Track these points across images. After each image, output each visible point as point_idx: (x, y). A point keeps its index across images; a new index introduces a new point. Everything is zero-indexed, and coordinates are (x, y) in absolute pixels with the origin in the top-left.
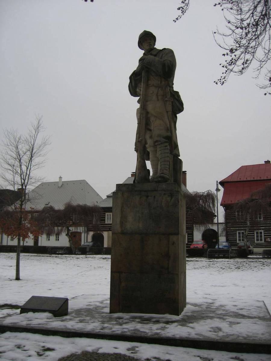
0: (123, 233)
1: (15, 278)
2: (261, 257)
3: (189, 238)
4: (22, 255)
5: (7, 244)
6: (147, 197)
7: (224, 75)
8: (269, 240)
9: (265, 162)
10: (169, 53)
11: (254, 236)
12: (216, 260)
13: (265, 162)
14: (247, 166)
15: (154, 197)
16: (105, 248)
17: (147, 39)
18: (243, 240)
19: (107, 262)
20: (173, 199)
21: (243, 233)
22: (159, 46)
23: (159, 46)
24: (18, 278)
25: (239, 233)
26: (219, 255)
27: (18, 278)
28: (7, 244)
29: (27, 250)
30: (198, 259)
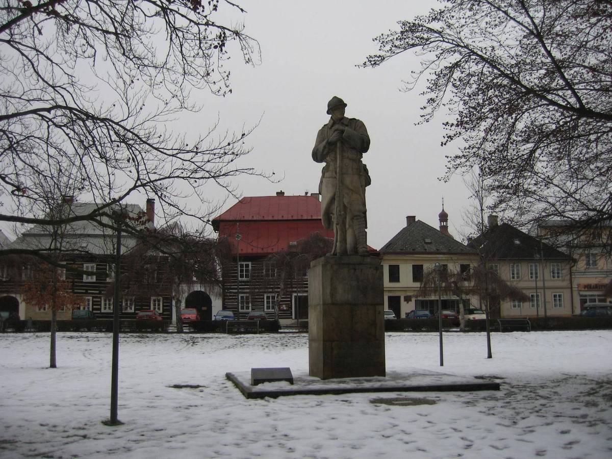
0: (333, 304)
1: (49, 364)
2: (297, 331)
3: (94, 307)
4: (59, 335)
5: (573, 312)
6: (355, 269)
7: (447, 174)
8: (285, 308)
9: (277, 193)
10: (357, 125)
11: (264, 301)
12: (242, 335)
13: (277, 193)
14: (251, 197)
15: (362, 270)
16: (487, 317)
17: (337, 106)
18: (273, 308)
19: (79, 343)
20: (378, 272)
21: (273, 298)
22: (349, 113)
23: (349, 113)
24: (53, 365)
25: (268, 298)
26: (238, 329)
27: (53, 365)
28: (573, 312)
29: (65, 327)
30: (211, 335)
